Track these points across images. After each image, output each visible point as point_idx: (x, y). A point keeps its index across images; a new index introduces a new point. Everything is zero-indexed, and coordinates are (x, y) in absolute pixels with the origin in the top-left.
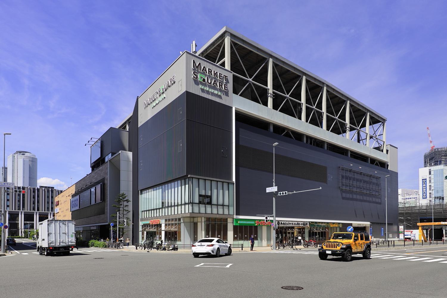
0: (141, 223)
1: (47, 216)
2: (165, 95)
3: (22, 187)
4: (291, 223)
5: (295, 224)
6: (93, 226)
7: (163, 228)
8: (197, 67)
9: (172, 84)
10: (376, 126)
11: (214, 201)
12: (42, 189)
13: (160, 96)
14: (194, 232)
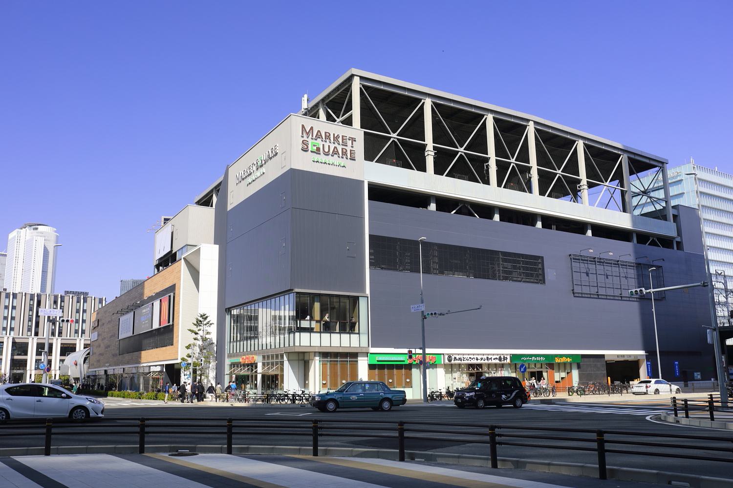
0: (228, 362)
1: (74, 346)
2: (264, 169)
3: (37, 294)
4: (475, 357)
5: (482, 359)
6: (156, 366)
7: (260, 369)
8: (308, 133)
12: (70, 296)
13: (257, 169)
14: (305, 375)
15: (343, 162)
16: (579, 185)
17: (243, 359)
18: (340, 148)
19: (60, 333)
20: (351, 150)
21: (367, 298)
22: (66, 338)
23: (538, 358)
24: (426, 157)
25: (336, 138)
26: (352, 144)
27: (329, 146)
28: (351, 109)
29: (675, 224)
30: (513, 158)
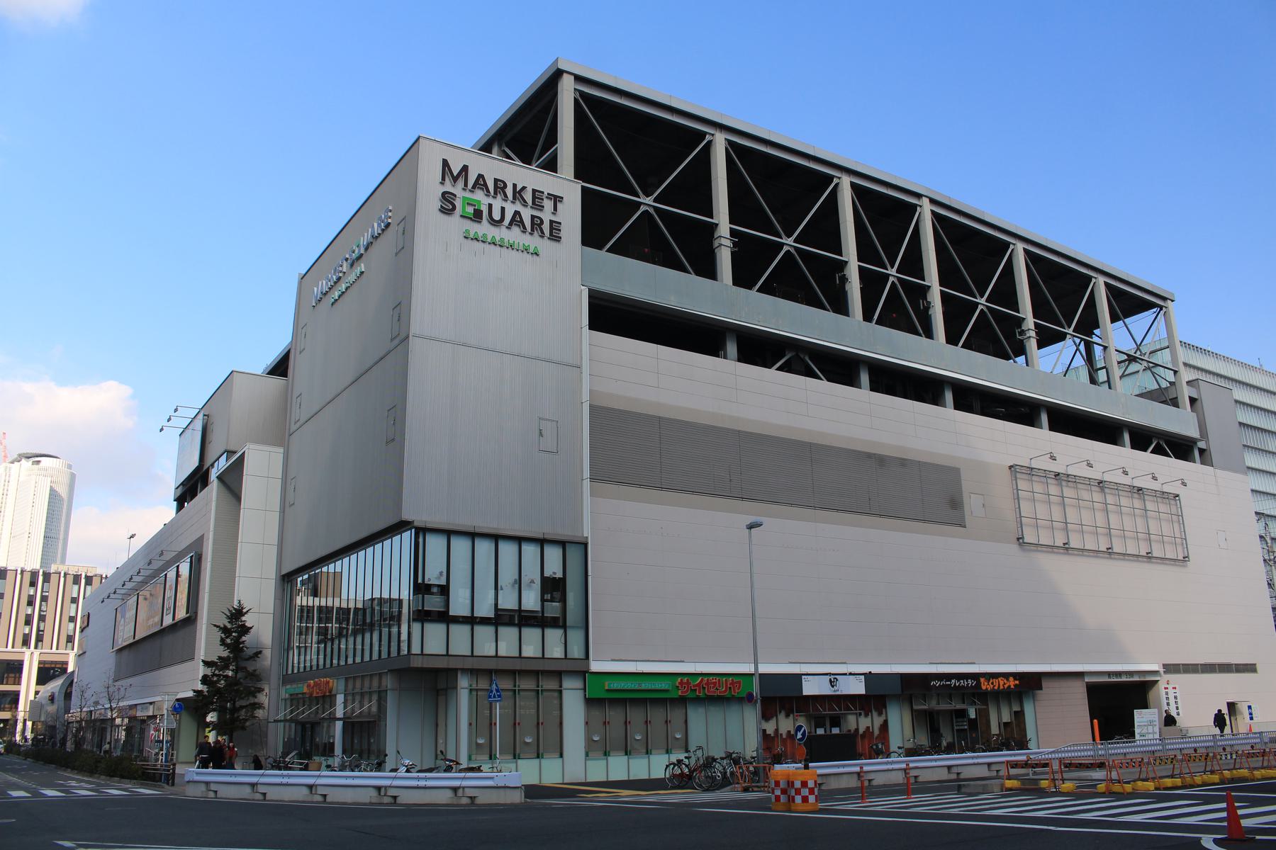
1: (64, 666)
2: (362, 265)
8: (455, 179)
9: (383, 230)
10: (1139, 322)
11: (459, 605)
13: (352, 265)
15: (533, 241)
16: (1019, 330)
17: (309, 686)
18: (526, 214)
19: (40, 639)
20: (551, 222)
21: (583, 546)
22: (49, 651)
23: (962, 681)
24: (716, 250)
25: (518, 194)
26: (555, 209)
27: (503, 209)
28: (555, 142)
29: (1194, 414)
30: (892, 268)
